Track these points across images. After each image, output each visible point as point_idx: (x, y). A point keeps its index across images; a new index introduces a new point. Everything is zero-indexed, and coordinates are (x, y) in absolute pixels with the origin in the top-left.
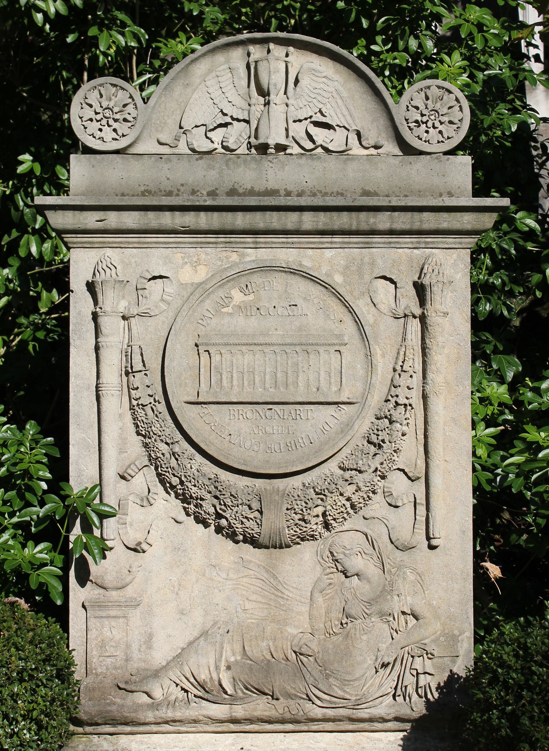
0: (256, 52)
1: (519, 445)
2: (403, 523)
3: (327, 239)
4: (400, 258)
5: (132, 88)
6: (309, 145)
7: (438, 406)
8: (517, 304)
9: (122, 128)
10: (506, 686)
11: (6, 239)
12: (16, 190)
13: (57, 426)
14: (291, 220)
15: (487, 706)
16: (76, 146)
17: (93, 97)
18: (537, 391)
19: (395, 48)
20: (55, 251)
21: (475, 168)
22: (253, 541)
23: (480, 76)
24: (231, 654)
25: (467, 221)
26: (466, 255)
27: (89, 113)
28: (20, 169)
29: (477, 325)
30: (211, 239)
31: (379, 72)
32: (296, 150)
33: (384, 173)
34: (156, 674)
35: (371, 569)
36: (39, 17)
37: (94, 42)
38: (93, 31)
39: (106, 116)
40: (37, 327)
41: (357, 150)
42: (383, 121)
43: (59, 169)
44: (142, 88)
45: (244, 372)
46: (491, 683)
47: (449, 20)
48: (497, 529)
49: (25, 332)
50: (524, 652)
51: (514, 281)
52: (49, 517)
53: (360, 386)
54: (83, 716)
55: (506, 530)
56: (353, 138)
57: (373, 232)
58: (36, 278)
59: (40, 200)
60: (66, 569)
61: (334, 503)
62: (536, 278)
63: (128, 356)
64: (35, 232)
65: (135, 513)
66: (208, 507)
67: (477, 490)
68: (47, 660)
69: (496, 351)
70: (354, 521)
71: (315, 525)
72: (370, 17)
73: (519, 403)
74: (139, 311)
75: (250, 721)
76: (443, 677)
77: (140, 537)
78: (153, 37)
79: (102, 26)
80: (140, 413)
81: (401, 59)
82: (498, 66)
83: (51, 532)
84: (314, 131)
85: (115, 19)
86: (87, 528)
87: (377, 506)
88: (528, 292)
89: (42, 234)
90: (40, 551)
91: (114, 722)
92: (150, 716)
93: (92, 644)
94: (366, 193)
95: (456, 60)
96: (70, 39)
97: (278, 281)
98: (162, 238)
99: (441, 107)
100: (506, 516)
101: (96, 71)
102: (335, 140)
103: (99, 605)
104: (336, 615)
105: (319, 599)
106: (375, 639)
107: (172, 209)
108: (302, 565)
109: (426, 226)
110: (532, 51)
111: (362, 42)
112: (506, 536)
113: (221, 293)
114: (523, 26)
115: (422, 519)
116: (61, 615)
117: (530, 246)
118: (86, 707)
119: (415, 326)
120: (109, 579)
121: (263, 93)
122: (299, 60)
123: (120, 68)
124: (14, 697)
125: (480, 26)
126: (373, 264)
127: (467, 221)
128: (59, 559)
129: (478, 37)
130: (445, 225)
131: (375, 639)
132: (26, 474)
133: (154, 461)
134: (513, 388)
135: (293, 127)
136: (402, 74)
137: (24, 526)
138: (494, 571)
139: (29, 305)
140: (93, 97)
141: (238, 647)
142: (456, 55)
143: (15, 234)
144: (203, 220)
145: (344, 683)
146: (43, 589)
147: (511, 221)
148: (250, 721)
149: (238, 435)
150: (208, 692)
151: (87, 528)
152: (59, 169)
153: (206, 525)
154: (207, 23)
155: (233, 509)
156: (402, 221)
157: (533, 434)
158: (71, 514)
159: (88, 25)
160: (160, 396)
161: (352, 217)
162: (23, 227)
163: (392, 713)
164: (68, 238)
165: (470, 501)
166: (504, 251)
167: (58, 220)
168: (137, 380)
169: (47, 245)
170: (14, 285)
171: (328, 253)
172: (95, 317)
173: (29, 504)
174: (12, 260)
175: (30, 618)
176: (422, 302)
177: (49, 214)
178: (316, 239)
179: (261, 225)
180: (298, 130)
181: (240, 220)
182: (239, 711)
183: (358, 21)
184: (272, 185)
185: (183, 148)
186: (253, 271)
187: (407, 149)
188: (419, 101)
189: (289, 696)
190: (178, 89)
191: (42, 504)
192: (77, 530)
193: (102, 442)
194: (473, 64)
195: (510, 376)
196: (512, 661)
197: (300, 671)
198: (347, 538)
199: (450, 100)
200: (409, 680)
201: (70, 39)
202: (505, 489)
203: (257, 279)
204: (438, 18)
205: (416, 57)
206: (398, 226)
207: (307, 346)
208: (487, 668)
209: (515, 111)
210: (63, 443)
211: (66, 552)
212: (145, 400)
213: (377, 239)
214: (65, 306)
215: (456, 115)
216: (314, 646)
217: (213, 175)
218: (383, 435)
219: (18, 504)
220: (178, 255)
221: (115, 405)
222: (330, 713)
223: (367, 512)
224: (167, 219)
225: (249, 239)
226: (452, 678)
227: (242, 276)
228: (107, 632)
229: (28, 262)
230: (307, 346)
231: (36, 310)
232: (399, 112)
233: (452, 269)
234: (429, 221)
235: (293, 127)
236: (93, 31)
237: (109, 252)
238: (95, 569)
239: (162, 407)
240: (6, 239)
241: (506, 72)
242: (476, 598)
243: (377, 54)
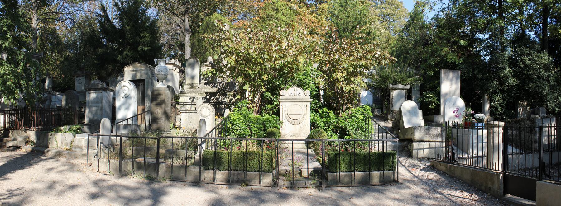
2: (305, 123)
4: (305, 103)
13: (279, 116)
33: (304, 97)
74: (286, 108)
83: (279, 124)
99: (308, 92)
108: (298, 126)
155: (293, 122)
161: (301, 100)
198: (301, 125)
221: (284, 115)
233: (309, 104)
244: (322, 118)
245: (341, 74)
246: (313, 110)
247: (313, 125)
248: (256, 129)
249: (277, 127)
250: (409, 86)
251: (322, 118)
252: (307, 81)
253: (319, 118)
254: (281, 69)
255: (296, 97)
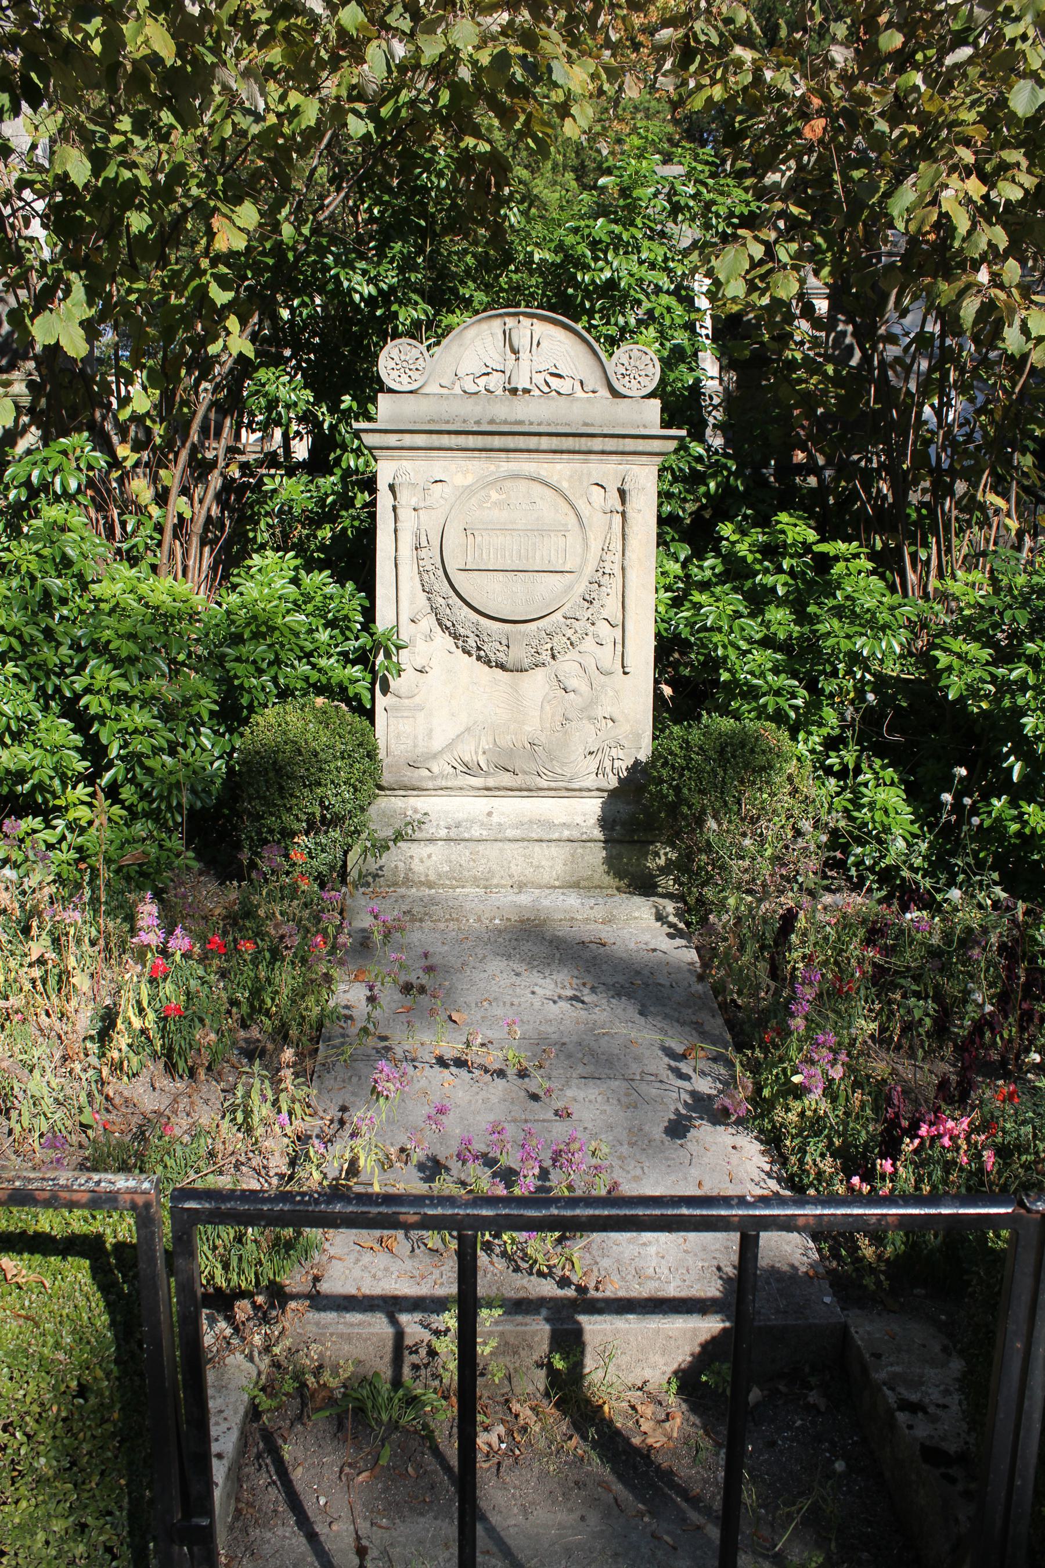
0: (510, 322)
1: (687, 605)
2: (607, 656)
3: (558, 456)
4: (609, 470)
5: (423, 348)
6: (546, 389)
7: (631, 574)
8: (691, 507)
9: (415, 375)
10: (673, 767)
11: (332, 456)
12: (340, 421)
13: (367, 585)
14: (532, 442)
15: (660, 781)
16: (382, 388)
17: (395, 353)
18: (701, 567)
19: (608, 323)
20: (367, 464)
21: (663, 410)
22: (502, 667)
23: (668, 345)
24: (486, 744)
25: (656, 445)
26: (655, 470)
27: (392, 364)
28: (343, 406)
29: (661, 521)
30: (476, 454)
31: (598, 340)
32: (536, 392)
33: (597, 410)
34: (435, 756)
35: (583, 687)
36: (357, 297)
37: (395, 315)
38: (395, 307)
39: (405, 368)
40: (354, 519)
41: (580, 394)
42: (599, 373)
43: (370, 407)
44: (429, 348)
45: (497, 549)
46: (664, 765)
47: (646, 305)
48: (670, 664)
49: (346, 520)
50: (686, 745)
51: (687, 491)
52: (362, 648)
53: (578, 560)
54: (384, 784)
55: (675, 665)
56: (578, 385)
57: (590, 452)
58: (353, 483)
59: (356, 425)
60: (373, 684)
61: (559, 642)
62: (702, 489)
63: (418, 537)
64: (353, 451)
65: (421, 646)
66: (472, 642)
67: (658, 635)
68: (360, 745)
69: (673, 540)
70: (572, 654)
71: (546, 656)
72: (591, 300)
73: (688, 576)
74: (427, 504)
75: (498, 789)
76: (630, 762)
77: (424, 662)
78: (437, 313)
79: (401, 303)
80: (425, 576)
81: (613, 331)
82: (681, 338)
84: (550, 379)
85: (409, 300)
86: (388, 655)
87: (589, 644)
88: (697, 500)
89: (358, 452)
90: (356, 671)
91: (405, 788)
92: (430, 785)
93: (391, 735)
94: (586, 424)
95: (652, 332)
96: (379, 313)
97: (523, 485)
98: (442, 453)
99: (640, 363)
100: (676, 655)
101: (396, 335)
102: (564, 386)
103: (396, 709)
104: (559, 718)
105: (547, 708)
106: (584, 736)
107: (449, 433)
108: (536, 684)
109: (627, 449)
110: (703, 332)
111: (585, 318)
112: (676, 669)
113: (483, 493)
114: (698, 310)
115: (619, 653)
116: (370, 715)
117: (699, 467)
118: (386, 779)
119: (619, 517)
120: (403, 692)
121: (515, 351)
122: (542, 329)
123: (415, 331)
124: (338, 769)
125: (669, 309)
126: (589, 474)
127: (656, 445)
128: (369, 677)
129: (667, 317)
130: (640, 449)
131: (584, 736)
132: (346, 618)
133: (434, 610)
134: (684, 566)
135: (535, 376)
136: (613, 342)
137: (344, 654)
138: (667, 691)
139: (348, 503)
140: (395, 353)
141: (491, 739)
142: (651, 329)
143: (339, 452)
144: (471, 441)
145: (563, 764)
146: (357, 697)
147: (686, 449)
148: (498, 789)
149: (493, 593)
150: (469, 769)
151: (388, 655)
152: (370, 407)
153: (470, 654)
154: (475, 304)
155: (488, 643)
156: (611, 444)
157: (697, 597)
158: (377, 646)
159: (391, 303)
160: (439, 565)
161: (576, 441)
162: (344, 448)
163: (595, 786)
164: (376, 453)
165: (653, 643)
166: (681, 470)
167: (369, 439)
168: (423, 553)
169: (361, 460)
170: (338, 488)
171: (558, 466)
172: (394, 508)
173: (348, 639)
174: (337, 470)
175: (349, 716)
176: (623, 502)
177: (363, 435)
178: (551, 456)
179: (512, 446)
180: (539, 379)
181: (497, 442)
182: (491, 782)
183: (582, 303)
184: (519, 417)
185: (457, 390)
186: (505, 478)
187: (615, 393)
188: (625, 360)
189: (525, 773)
190: (454, 349)
191: (357, 639)
192: (381, 657)
193: (400, 594)
194: (663, 336)
195: (682, 557)
196: (678, 751)
197: (533, 756)
198: (567, 666)
199: (646, 359)
200: (607, 764)
201: (379, 313)
202: (677, 636)
203: (508, 484)
204: (639, 303)
205: (623, 330)
206: (608, 448)
207: (542, 531)
208: (661, 756)
209: (691, 370)
210: (371, 596)
211: (373, 671)
212: (429, 567)
213: (592, 457)
214: (373, 504)
215: (650, 370)
216: (543, 739)
217: (478, 410)
218: (594, 595)
219: (340, 638)
220: (453, 466)
222: (553, 785)
223: (581, 648)
224: (446, 440)
225: (503, 455)
226: (637, 763)
227: (497, 482)
228: (401, 727)
229: (348, 472)
230: (542, 531)
231: (353, 506)
232: (610, 365)
233: (645, 480)
234: (630, 445)
235: (535, 376)
236: (395, 307)
237: (404, 463)
238: (393, 684)
239: (441, 573)
240: (332, 456)
241: (686, 342)
242: (655, 709)
243: (596, 327)
244: (758, 600)
245: (975, 187)
246: (687, 530)
247: (688, 680)
248: (139, 718)
249: (339, 692)
250: (230, 295)
251: (758, 600)
252: (619, 267)
253: (736, 602)
254: (400, 140)
255: (527, 411)
